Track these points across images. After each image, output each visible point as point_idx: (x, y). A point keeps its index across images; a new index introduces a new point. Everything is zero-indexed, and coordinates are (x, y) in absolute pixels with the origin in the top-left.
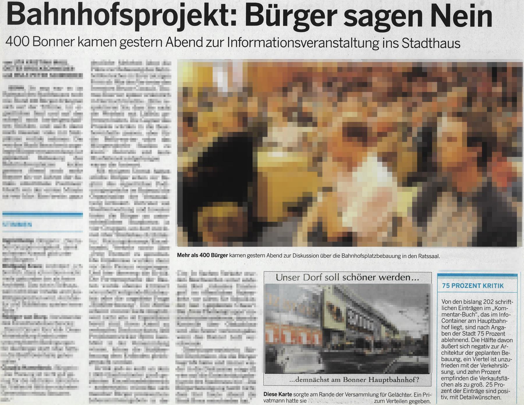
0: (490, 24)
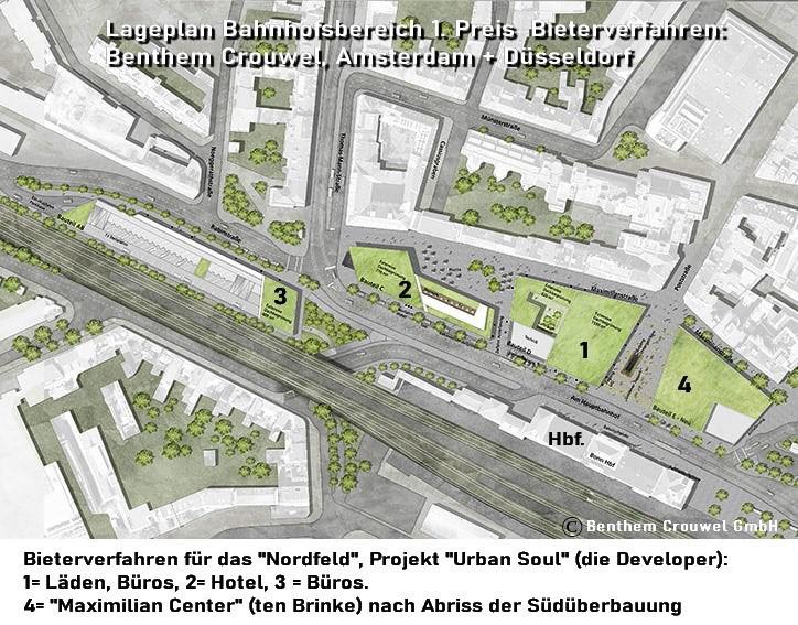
0: (509, 564)
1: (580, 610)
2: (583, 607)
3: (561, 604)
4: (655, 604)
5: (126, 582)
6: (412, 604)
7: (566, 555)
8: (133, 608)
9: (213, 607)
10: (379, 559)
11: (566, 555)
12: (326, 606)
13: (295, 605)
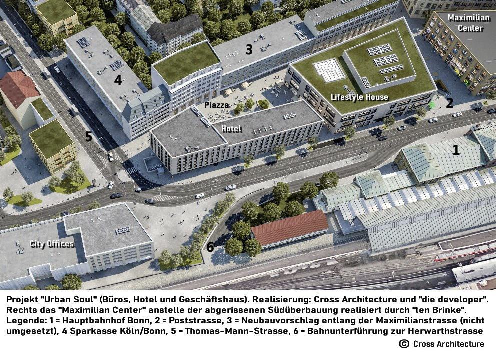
1: (292, 312)
2: (293, 311)
3: (283, 309)
4: (326, 309)
5: (106, 299)
6: (408, 309)
7: (95, 298)
8: (410, 322)
9: (132, 311)
10: (10, 299)
11: (95, 298)
12: (448, 310)
13: (434, 310)
